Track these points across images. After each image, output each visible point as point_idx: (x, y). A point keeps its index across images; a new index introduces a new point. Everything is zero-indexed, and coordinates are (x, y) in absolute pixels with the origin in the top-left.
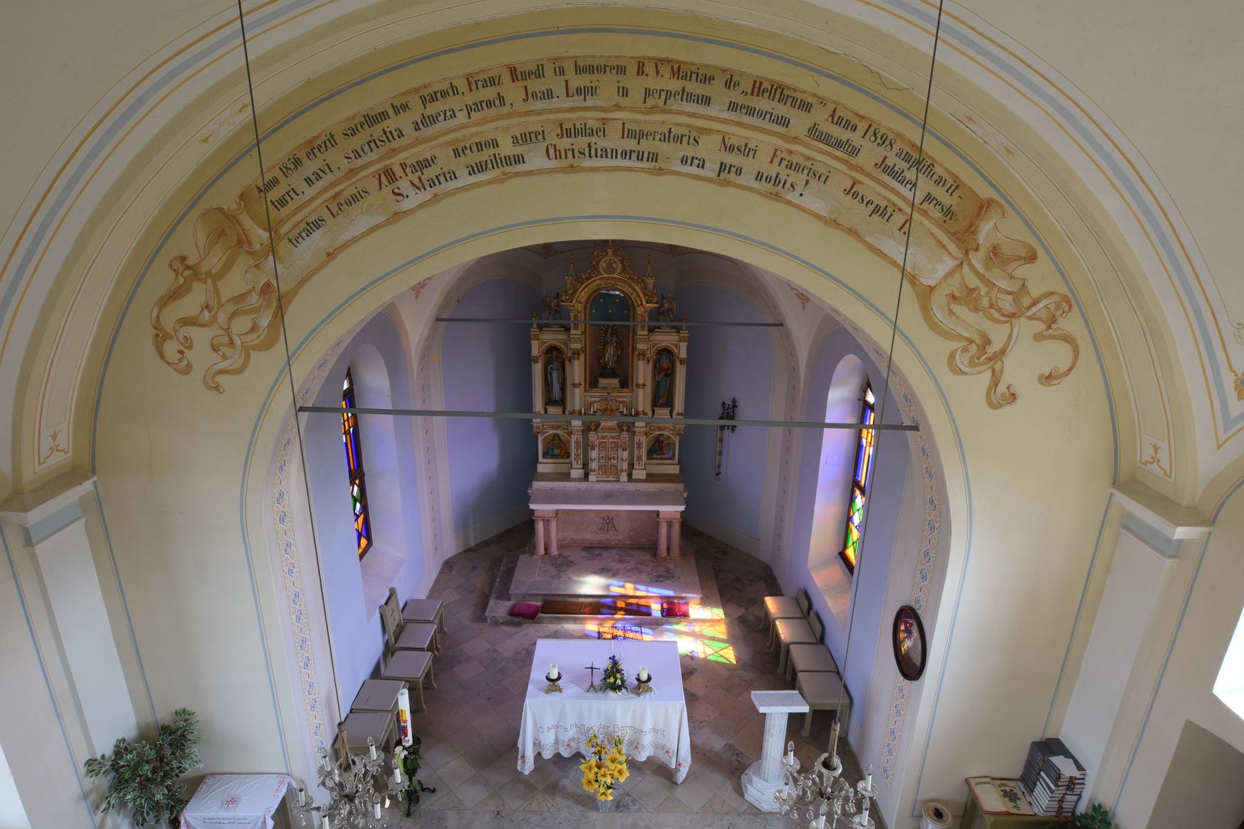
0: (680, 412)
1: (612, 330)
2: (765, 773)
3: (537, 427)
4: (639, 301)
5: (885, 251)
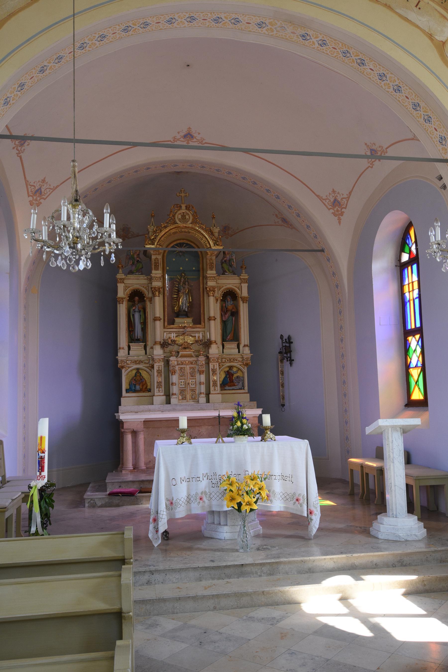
0: (246, 344)
1: (185, 279)
2: (392, 510)
3: (122, 361)
4: (208, 245)
5: (409, 18)
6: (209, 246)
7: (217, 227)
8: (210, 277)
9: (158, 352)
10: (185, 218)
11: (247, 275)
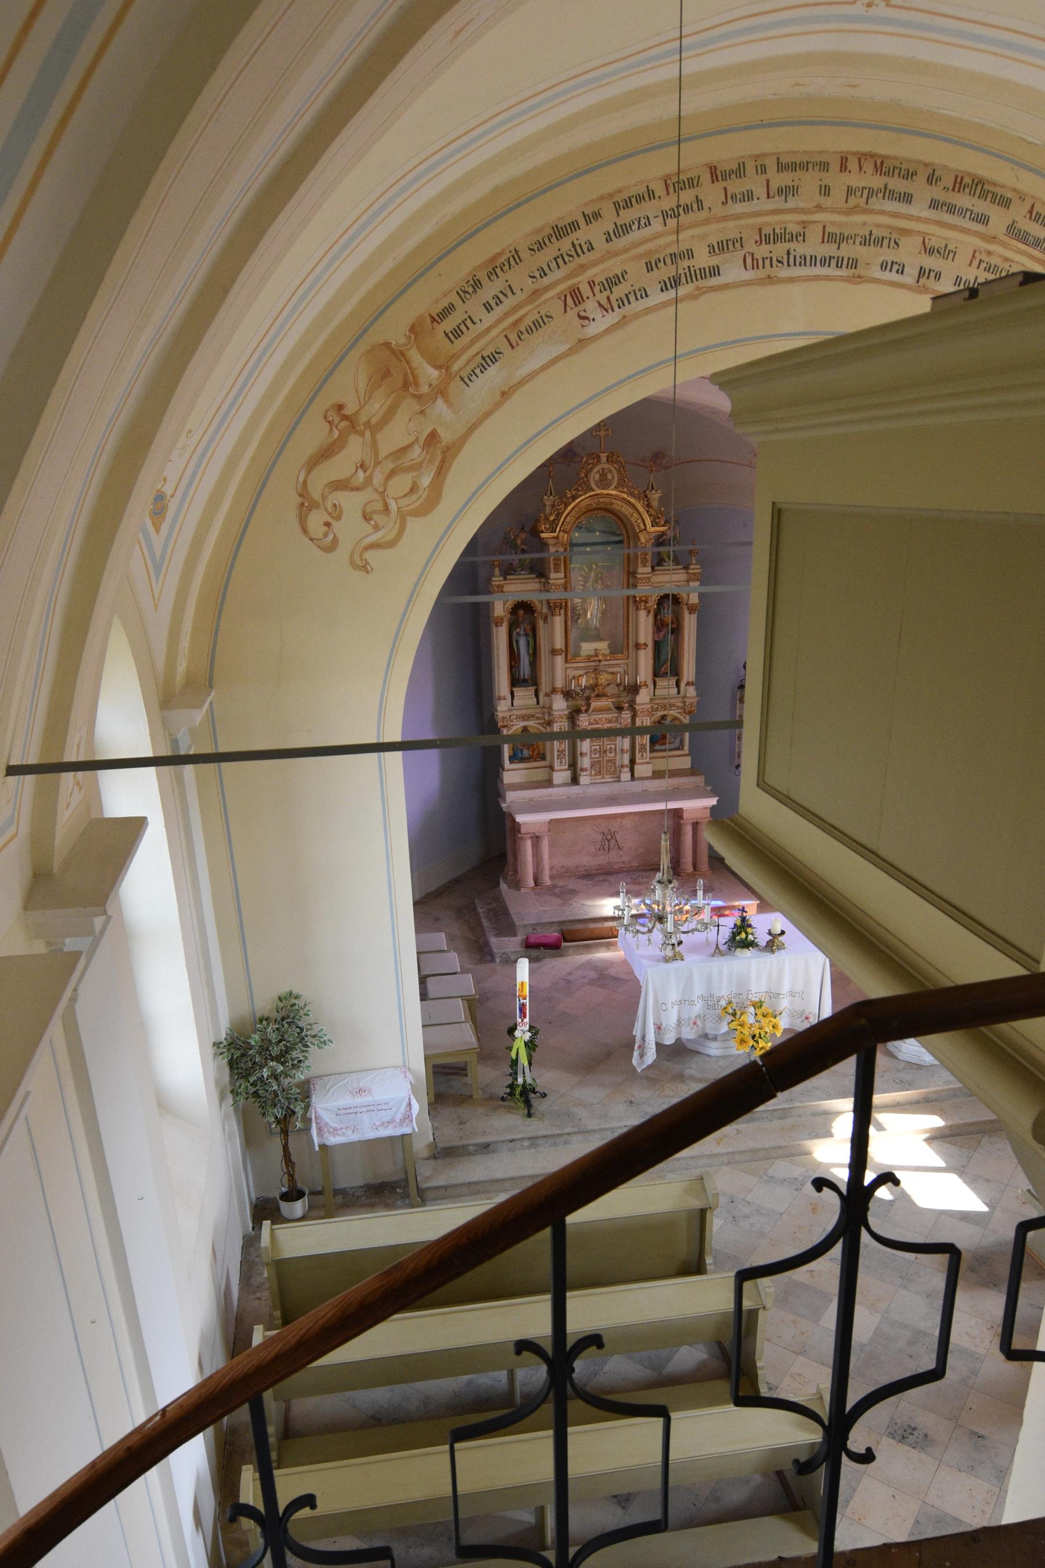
0: (691, 680)
3: (504, 718)
6: (643, 527)
7: (657, 491)
8: (643, 579)
9: (560, 705)
10: (606, 479)
11: (699, 567)
